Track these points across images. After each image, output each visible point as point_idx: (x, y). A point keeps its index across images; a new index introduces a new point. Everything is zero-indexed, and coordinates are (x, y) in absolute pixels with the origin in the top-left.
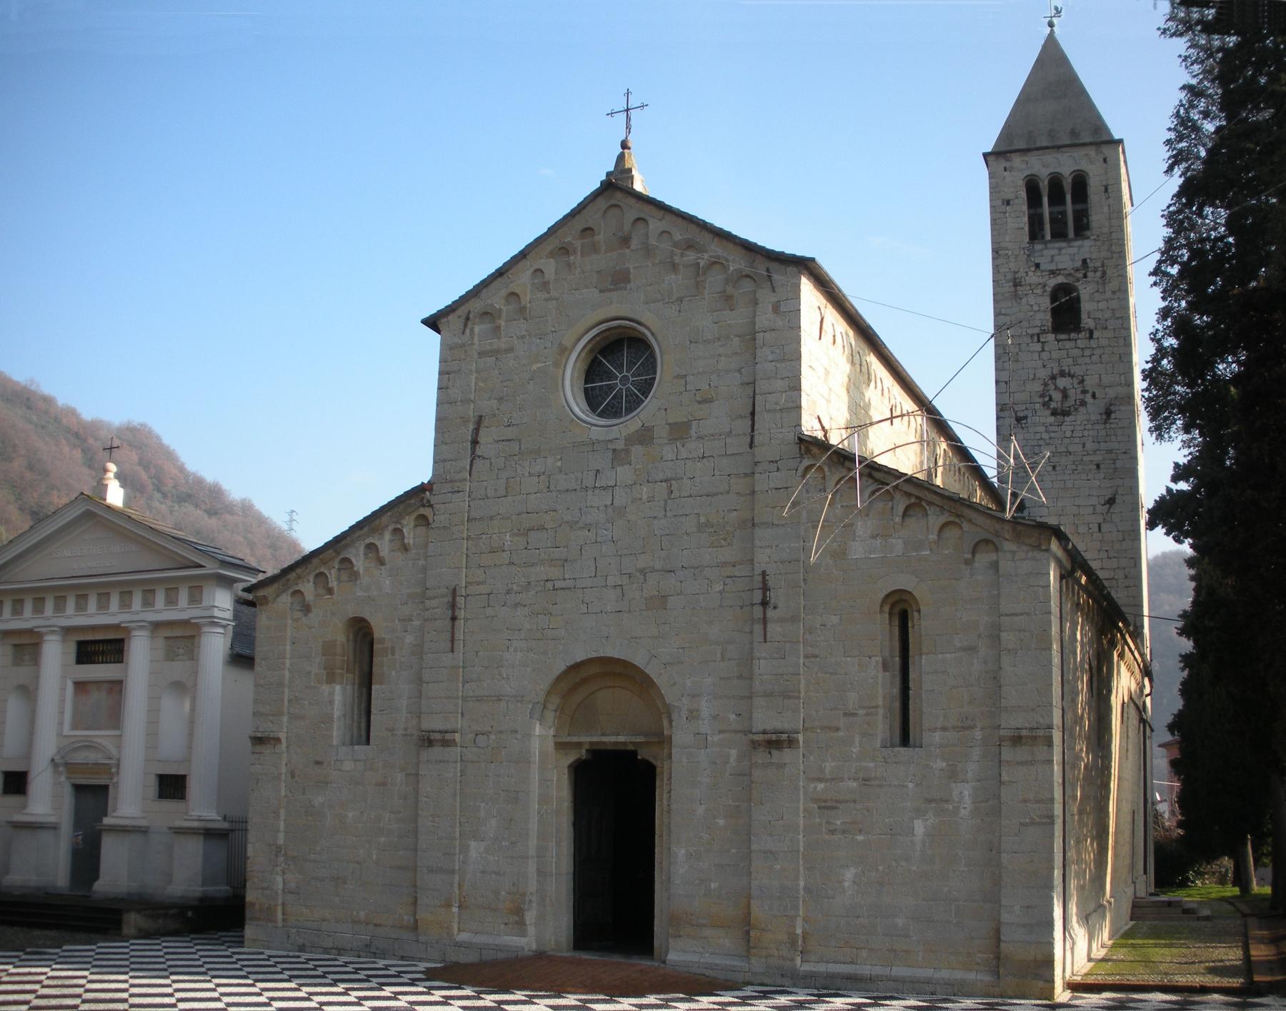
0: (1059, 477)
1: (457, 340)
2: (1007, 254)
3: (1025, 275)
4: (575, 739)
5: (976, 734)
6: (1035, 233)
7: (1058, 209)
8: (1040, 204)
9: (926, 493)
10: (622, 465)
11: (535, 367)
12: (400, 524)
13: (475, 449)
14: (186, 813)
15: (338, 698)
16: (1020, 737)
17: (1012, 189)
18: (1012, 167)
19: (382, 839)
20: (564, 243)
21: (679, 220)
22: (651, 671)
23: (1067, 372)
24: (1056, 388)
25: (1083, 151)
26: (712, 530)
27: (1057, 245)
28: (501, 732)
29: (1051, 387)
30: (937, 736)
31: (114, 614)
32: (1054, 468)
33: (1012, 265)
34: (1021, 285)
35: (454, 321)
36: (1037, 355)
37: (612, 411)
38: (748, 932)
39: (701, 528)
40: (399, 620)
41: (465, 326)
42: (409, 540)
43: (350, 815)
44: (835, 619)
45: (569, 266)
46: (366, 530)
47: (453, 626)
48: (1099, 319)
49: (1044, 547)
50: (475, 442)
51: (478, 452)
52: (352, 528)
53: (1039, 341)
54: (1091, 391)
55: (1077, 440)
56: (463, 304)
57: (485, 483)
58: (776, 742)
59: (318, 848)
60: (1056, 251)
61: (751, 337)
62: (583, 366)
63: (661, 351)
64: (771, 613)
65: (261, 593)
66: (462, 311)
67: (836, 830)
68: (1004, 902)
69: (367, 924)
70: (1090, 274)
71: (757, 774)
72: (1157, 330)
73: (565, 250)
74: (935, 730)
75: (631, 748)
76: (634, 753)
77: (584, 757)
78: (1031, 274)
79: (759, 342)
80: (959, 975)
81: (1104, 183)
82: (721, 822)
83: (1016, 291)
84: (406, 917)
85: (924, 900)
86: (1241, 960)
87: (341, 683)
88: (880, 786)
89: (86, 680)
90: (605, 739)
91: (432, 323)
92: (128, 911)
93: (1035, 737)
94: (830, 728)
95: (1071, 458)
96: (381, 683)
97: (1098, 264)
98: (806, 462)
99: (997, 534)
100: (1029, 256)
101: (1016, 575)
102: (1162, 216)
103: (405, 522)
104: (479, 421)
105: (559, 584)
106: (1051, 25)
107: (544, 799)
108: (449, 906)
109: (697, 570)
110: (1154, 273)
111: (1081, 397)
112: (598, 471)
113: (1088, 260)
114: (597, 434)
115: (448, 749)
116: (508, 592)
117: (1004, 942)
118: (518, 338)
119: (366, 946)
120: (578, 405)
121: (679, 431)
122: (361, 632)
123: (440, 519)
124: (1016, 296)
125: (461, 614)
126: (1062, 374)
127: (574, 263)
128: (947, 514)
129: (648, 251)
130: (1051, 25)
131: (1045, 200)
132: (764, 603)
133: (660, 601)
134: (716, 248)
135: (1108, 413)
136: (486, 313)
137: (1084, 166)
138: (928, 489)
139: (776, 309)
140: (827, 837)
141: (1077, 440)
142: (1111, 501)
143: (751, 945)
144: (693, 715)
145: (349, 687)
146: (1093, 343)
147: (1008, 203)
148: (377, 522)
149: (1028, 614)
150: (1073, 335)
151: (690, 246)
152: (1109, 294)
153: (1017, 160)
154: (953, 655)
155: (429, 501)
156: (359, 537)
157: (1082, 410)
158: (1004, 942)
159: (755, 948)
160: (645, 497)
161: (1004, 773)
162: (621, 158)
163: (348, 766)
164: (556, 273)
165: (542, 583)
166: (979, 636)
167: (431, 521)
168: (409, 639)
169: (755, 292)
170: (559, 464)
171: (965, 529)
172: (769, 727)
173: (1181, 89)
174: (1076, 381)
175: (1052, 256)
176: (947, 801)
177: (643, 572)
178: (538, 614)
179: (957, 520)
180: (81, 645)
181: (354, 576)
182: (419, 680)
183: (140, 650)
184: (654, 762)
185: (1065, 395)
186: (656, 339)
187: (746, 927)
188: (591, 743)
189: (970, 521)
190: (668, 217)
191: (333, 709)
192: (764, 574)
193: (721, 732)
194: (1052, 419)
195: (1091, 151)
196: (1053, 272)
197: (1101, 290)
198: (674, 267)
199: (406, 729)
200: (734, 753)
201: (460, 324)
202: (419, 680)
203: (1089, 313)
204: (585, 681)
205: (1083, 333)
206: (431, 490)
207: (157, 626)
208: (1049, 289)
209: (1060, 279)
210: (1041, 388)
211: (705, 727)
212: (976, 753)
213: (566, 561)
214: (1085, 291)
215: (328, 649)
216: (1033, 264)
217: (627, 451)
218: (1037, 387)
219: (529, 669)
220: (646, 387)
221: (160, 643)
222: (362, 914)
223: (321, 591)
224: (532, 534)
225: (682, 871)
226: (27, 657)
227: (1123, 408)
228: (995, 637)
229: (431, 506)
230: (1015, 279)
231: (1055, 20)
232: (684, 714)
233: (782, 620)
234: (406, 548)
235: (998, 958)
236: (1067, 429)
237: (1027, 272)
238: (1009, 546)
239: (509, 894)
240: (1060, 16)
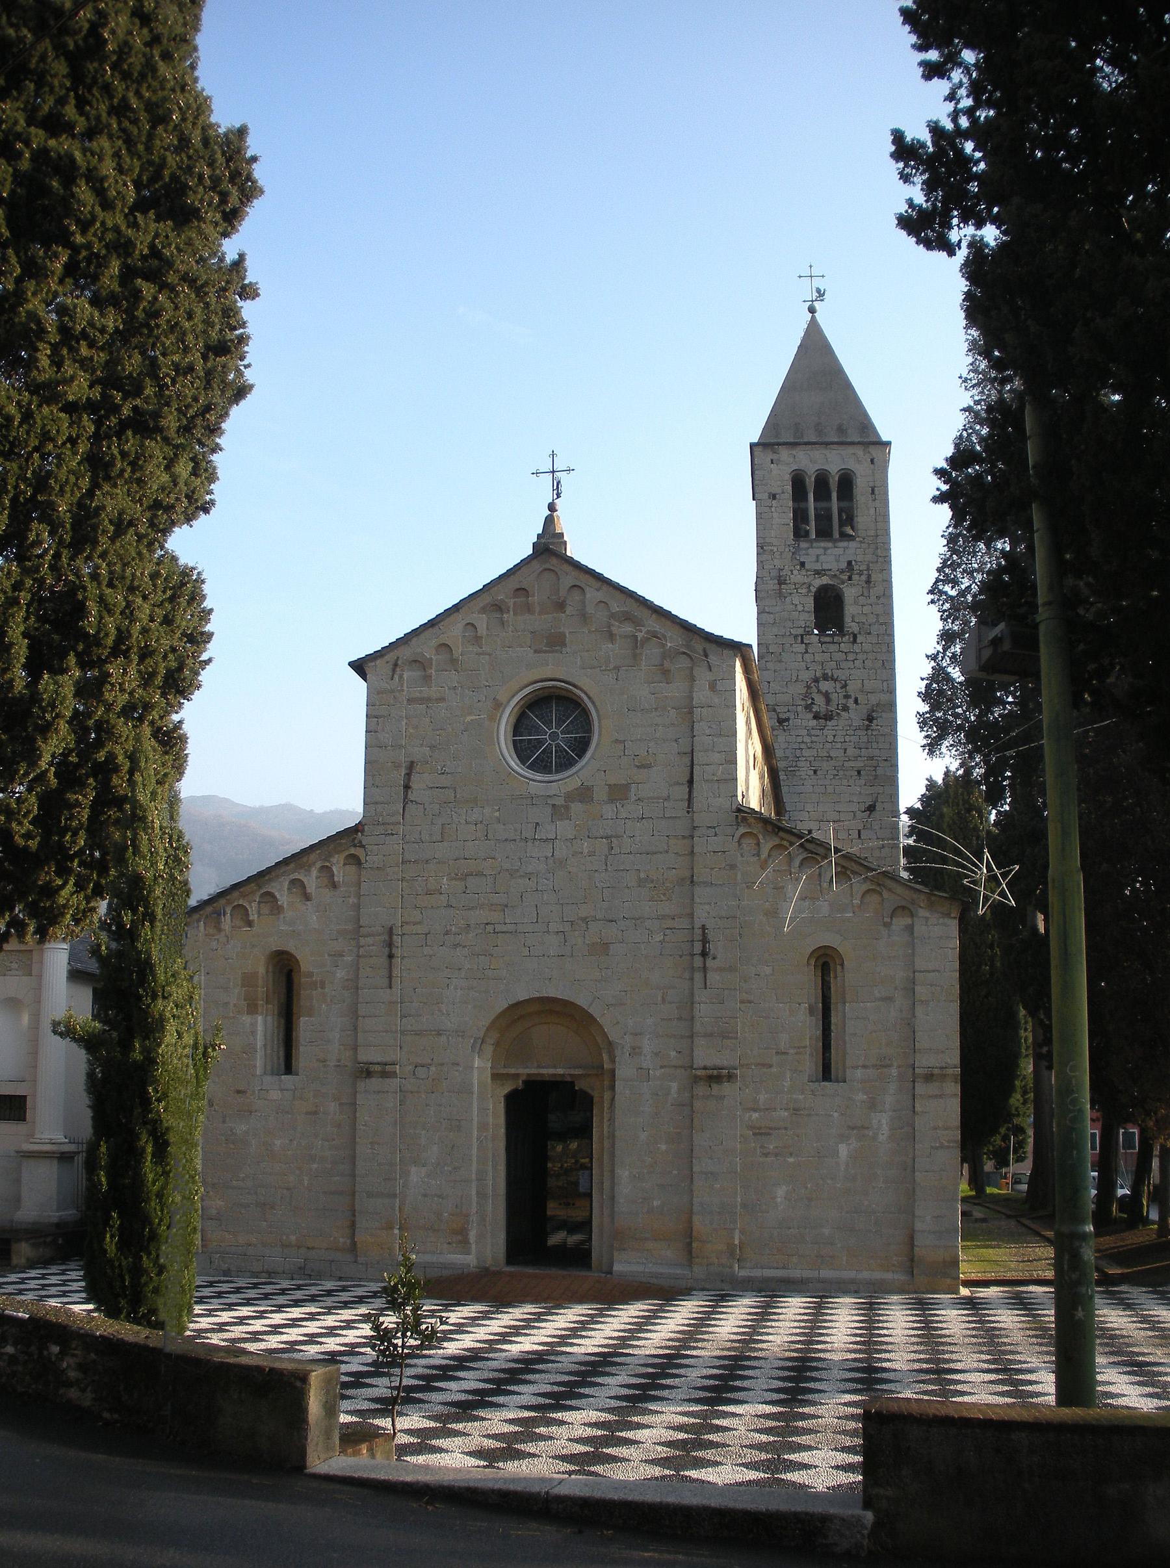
0: (820, 782)
2: (772, 550)
3: (789, 573)
4: (513, 1071)
6: (799, 533)
7: (824, 505)
8: (805, 498)
9: (853, 864)
11: (469, 718)
12: (329, 861)
13: (407, 792)
14: (32, 1135)
15: (260, 1028)
16: (932, 1075)
18: (779, 460)
19: (315, 1166)
20: (497, 600)
21: (618, 593)
22: (594, 1011)
23: (830, 674)
24: (819, 691)
25: (851, 450)
26: (652, 885)
27: (822, 544)
28: (442, 1064)
29: (814, 690)
30: (859, 1073)
32: (815, 772)
33: (777, 563)
36: (800, 655)
37: (542, 765)
38: (690, 1244)
39: (641, 883)
40: (329, 955)
41: (394, 671)
42: (338, 877)
43: (278, 1142)
44: (768, 970)
45: (502, 623)
46: (292, 865)
47: (391, 962)
48: (864, 623)
49: (952, 915)
50: (407, 787)
51: (411, 796)
52: (278, 864)
53: (802, 642)
54: (853, 697)
55: (839, 745)
56: (392, 650)
57: (419, 828)
58: (716, 1077)
60: (822, 551)
61: (688, 711)
62: (513, 720)
63: (599, 716)
66: (391, 657)
67: (769, 1153)
68: (917, 1213)
69: (299, 1247)
70: (855, 577)
71: (698, 1104)
72: (938, 652)
73: (498, 607)
74: (857, 1067)
75: (569, 1079)
76: (572, 1084)
79: (696, 717)
80: (878, 1275)
81: (871, 484)
82: (663, 1147)
83: (780, 589)
85: (847, 1212)
86: (1051, 1258)
87: (262, 1014)
88: (809, 1115)
90: (544, 1071)
91: (359, 667)
92: (19, 1240)
93: (945, 1075)
94: (763, 1065)
95: (832, 763)
97: (863, 567)
99: (913, 902)
100: (793, 553)
102: (942, 536)
103: (334, 860)
104: (411, 766)
105: (499, 928)
106: (812, 310)
107: (483, 1127)
108: (392, 1228)
109: (638, 921)
110: (931, 592)
111: (844, 701)
112: (537, 824)
113: (853, 563)
114: (535, 788)
115: (388, 1080)
116: (447, 933)
118: (449, 689)
119: (300, 1268)
121: (618, 793)
123: (372, 859)
124: (781, 595)
125: (397, 952)
126: (825, 677)
127: (508, 621)
128: (869, 883)
129: (584, 617)
130: (812, 310)
132: (704, 954)
133: (603, 948)
134: (653, 624)
135: (870, 719)
136: (415, 661)
137: (851, 465)
138: (891, 878)
139: (713, 686)
140: (761, 1159)
141: (839, 745)
142: (871, 808)
143: (694, 1255)
144: (635, 1051)
145: (269, 1018)
146: (857, 648)
147: (774, 497)
148: (305, 859)
151: (627, 618)
152: (873, 599)
153: (784, 454)
155: (360, 842)
156: (284, 872)
159: (698, 1257)
160: (586, 851)
161: (917, 1105)
162: (549, 522)
163: (275, 1095)
164: (488, 629)
165: (482, 926)
166: (896, 988)
167: (363, 861)
168: (340, 974)
169: (692, 669)
170: (497, 814)
173: (961, 410)
174: (838, 685)
175: (818, 556)
176: (868, 1128)
177: (585, 920)
178: (478, 955)
181: (276, 909)
182: (354, 1014)
184: (590, 1091)
185: (828, 701)
186: (593, 703)
187: (688, 1241)
188: (528, 1075)
189: (890, 890)
190: (605, 588)
191: (255, 1039)
192: (703, 928)
193: (662, 1067)
195: (859, 451)
196: (818, 573)
197: (866, 594)
198: (611, 637)
199: (339, 1061)
200: (674, 1086)
201: (387, 670)
202: (354, 1014)
203: (853, 617)
204: (521, 1017)
206: (362, 831)
208: (813, 590)
209: (825, 580)
210: (804, 691)
212: (892, 1087)
214: (850, 593)
215: (248, 980)
216: (798, 562)
217: (567, 808)
218: (800, 689)
220: (581, 746)
222: (293, 1238)
223: (238, 923)
227: (884, 715)
228: (910, 989)
229: (363, 846)
230: (780, 576)
231: (816, 304)
233: (720, 970)
234: (334, 886)
235: (912, 1260)
236: (829, 733)
237: (792, 571)
238: (922, 913)
239: (453, 1215)
240: (822, 300)
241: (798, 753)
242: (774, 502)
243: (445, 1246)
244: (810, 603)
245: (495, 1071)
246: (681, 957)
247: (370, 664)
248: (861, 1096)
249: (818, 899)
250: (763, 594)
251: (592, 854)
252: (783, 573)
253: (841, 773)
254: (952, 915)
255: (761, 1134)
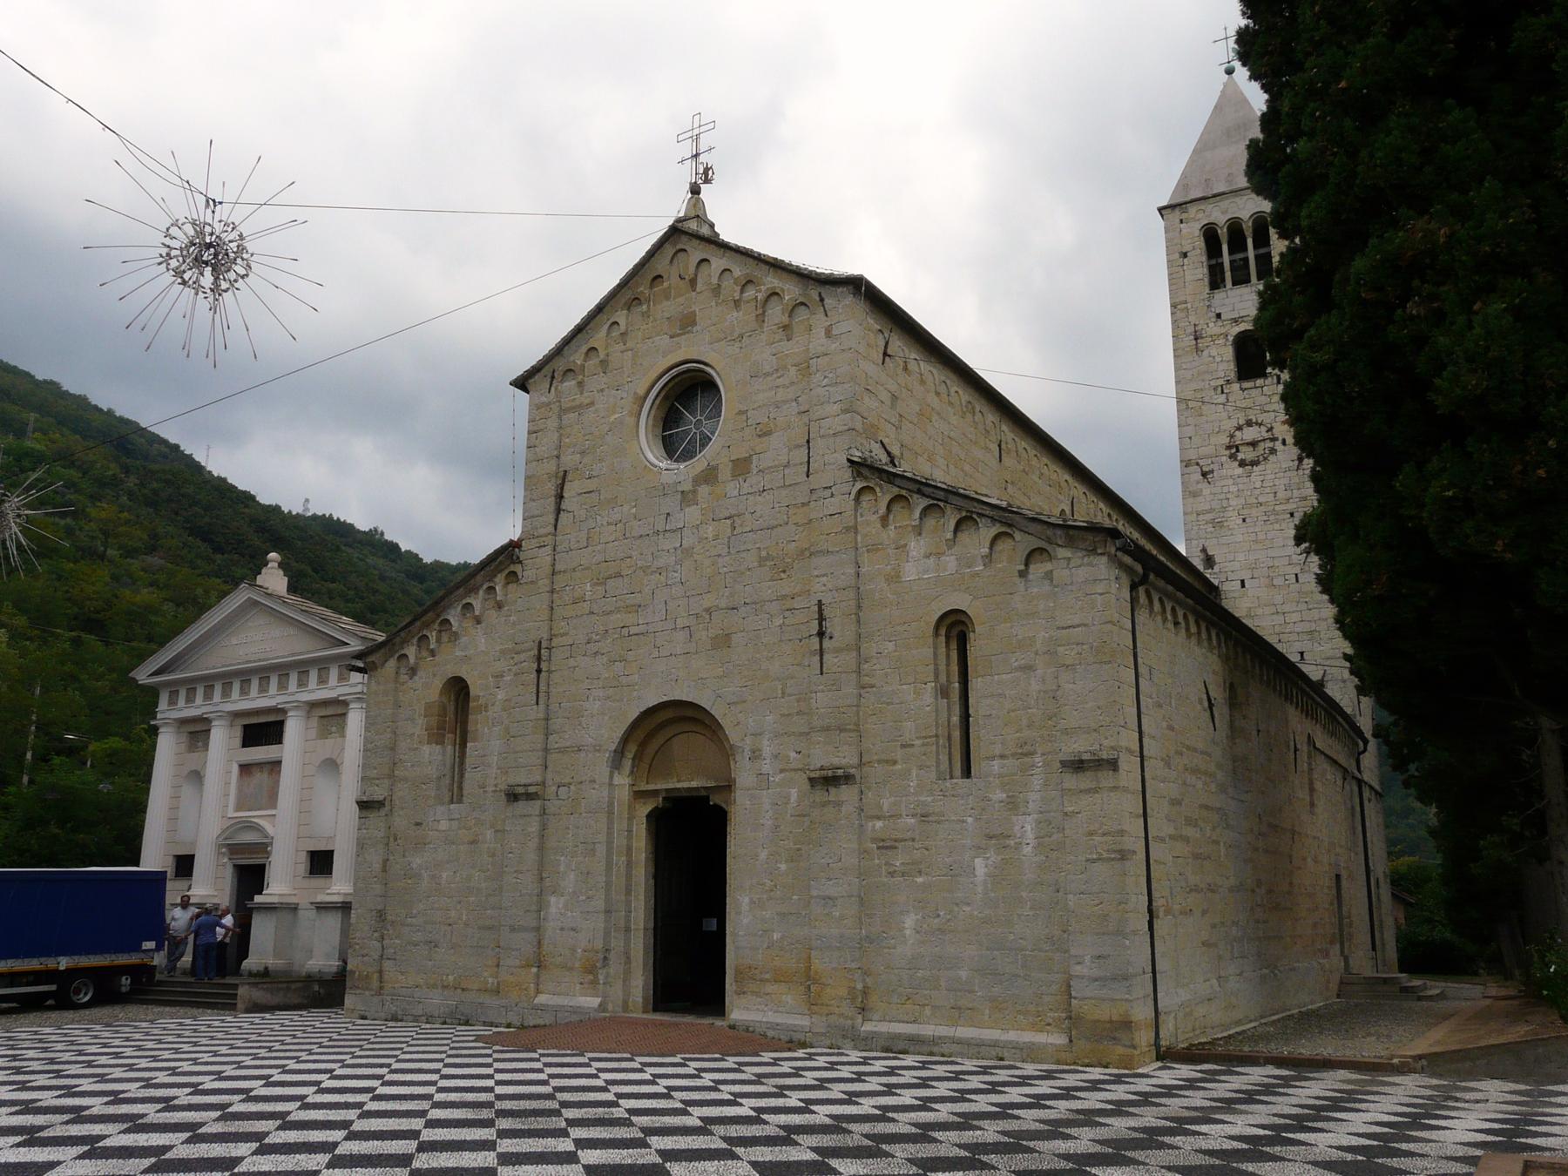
1: (544, 399)
4: (651, 787)
5: (1037, 760)
6: (1216, 282)
10: (689, 506)
17: (1189, 241)
23: (1254, 420)
31: (272, 697)
32: (1244, 520)
33: (1193, 319)
34: (1202, 338)
35: (540, 382)
37: (688, 455)
39: (762, 561)
43: (444, 875)
44: (891, 646)
49: (1099, 551)
53: (1223, 392)
54: (1280, 438)
59: (415, 912)
64: (827, 643)
65: (370, 659)
66: (547, 370)
67: (895, 871)
69: (456, 988)
74: (993, 758)
75: (704, 793)
76: (707, 798)
77: (660, 806)
78: (1211, 325)
82: (783, 867)
83: (1197, 344)
84: (490, 980)
89: (250, 762)
94: (887, 761)
95: (1262, 509)
96: (474, 740)
98: (859, 485)
101: (1072, 584)
103: (497, 580)
105: (634, 630)
112: (668, 514)
114: (667, 478)
117: (1075, 998)
118: (598, 391)
120: (652, 452)
122: (458, 688)
128: (998, 525)
131: (1225, 248)
132: (821, 634)
133: (723, 641)
134: (772, 281)
141: (1268, 490)
144: (756, 755)
145: (450, 748)
149: (1085, 625)
150: (1259, 382)
154: (1009, 676)
155: (518, 558)
157: (1272, 458)
158: (1075, 998)
163: (444, 825)
171: (1017, 539)
172: (825, 763)
177: (708, 610)
179: (1009, 531)
180: (246, 728)
183: (293, 728)
184: (724, 806)
193: (782, 771)
194: (1240, 470)
196: (1236, 321)
199: (496, 786)
204: (662, 726)
205: (1270, 379)
207: (313, 705)
208: (1231, 338)
211: (766, 767)
213: (640, 606)
216: (1214, 314)
217: (694, 492)
219: (606, 718)
221: (314, 722)
222: (451, 978)
224: (610, 582)
225: (745, 921)
226: (200, 744)
229: (520, 562)
230: (1196, 332)
232: (747, 754)
238: (1063, 553)
241: (1225, 503)
242: (1186, 260)
243: (578, 986)
244: (1229, 352)
245: (636, 789)
246: (801, 640)
247: (530, 381)
248: (1000, 795)
249: (944, 554)
250: (1180, 352)
251: (716, 538)
252: (1198, 328)
253: (1272, 518)
254: (1099, 551)
255: (886, 848)
